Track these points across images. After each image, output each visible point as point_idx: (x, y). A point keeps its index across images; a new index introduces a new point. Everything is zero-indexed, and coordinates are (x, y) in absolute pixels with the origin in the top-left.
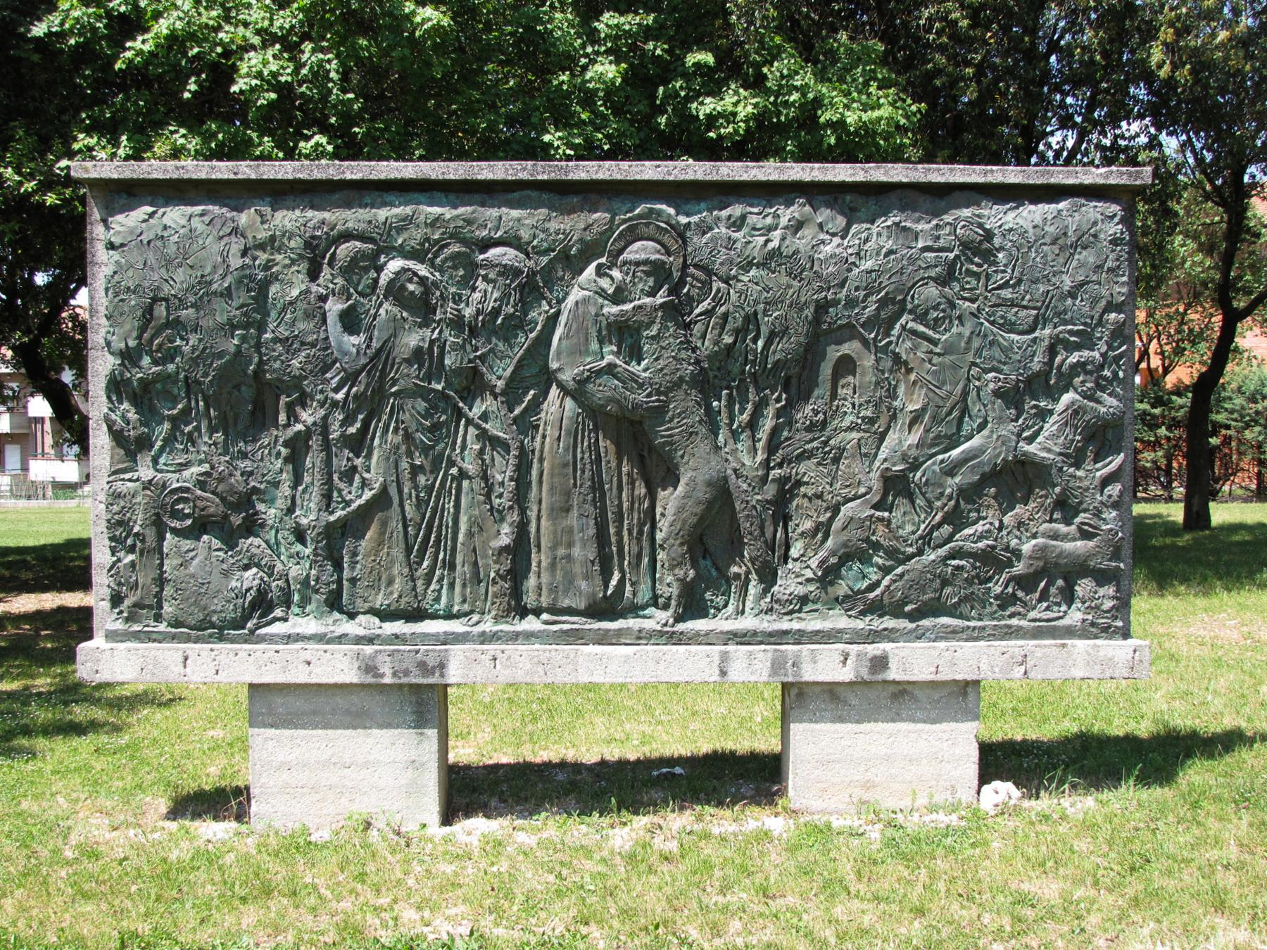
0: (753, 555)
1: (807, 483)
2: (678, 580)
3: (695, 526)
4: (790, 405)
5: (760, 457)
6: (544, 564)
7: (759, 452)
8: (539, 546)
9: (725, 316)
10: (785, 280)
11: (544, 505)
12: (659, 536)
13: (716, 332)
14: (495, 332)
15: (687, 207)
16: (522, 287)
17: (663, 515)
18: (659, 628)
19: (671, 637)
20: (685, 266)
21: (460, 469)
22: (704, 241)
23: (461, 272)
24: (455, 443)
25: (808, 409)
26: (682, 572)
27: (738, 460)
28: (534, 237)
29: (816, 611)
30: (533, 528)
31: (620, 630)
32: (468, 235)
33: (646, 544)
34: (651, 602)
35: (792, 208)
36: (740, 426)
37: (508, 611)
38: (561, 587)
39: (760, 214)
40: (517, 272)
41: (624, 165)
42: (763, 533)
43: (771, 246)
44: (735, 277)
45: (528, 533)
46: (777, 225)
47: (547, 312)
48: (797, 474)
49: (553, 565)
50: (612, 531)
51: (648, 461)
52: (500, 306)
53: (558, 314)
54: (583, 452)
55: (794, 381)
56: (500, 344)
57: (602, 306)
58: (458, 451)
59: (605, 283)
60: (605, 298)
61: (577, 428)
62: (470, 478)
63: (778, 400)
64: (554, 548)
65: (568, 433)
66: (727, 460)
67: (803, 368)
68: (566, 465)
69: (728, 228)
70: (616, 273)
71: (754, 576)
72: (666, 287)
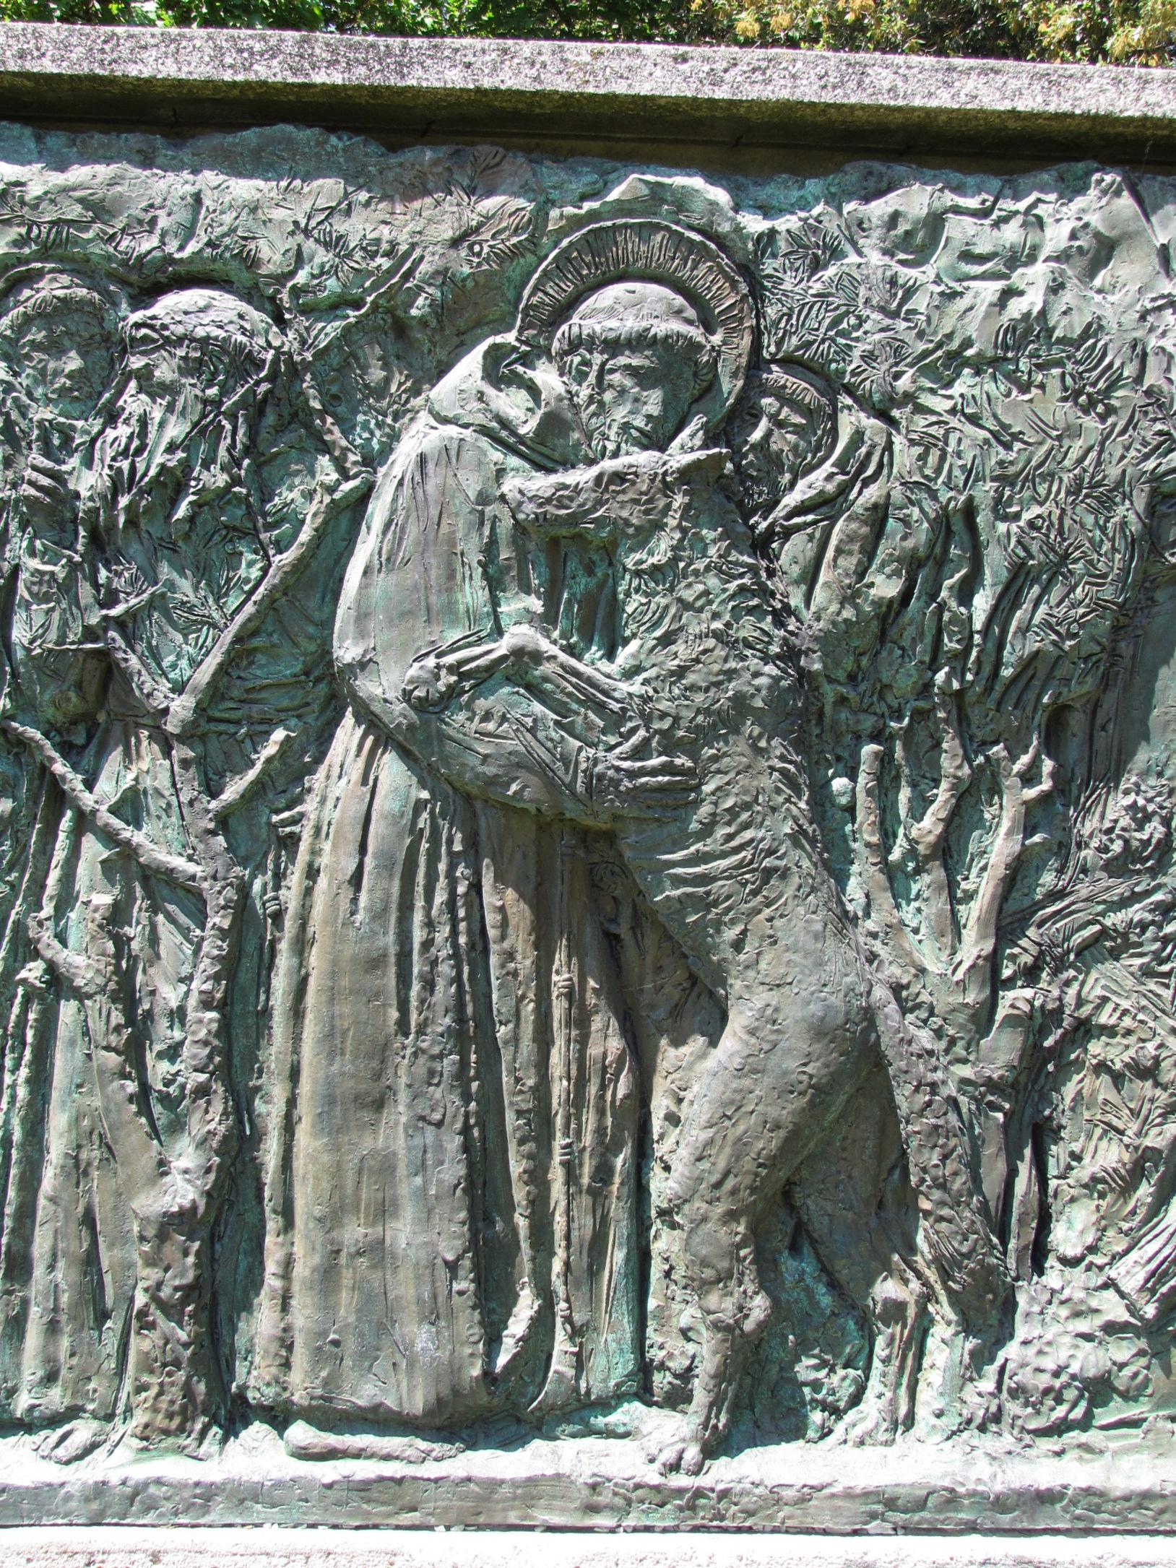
0: (947, 1250)
1: (1111, 1031)
2: (717, 1326)
3: (772, 1163)
4: (1064, 790)
5: (973, 947)
6: (301, 1271)
7: (969, 934)
8: (287, 1212)
9: (879, 515)
10: (1058, 411)
11: (305, 1087)
12: (662, 1187)
13: (849, 563)
14: (167, 547)
15: (770, 192)
16: (256, 409)
17: (673, 1119)
18: (652, 1476)
19: (692, 1507)
20: (756, 363)
21: (51, 968)
22: (817, 287)
23: (73, 362)
24: (38, 885)
25: (1117, 806)
26: (729, 1304)
27: (906, 958)
28: (300, 259)
29: (1134, 1423)
30: (270, 1154)
31: (531, 1481)
32: (97, 249)
33: (618, 1210)
34: (633, 1386)
35: (1080, 202)
36: (912, 853)
37: (186, 1415)
38: (351, 1344)
39: (984, 213)
40: (243, 362)
41: (580, 51)
42: (976, 1180)
43: (1016, 308)
44: (909, 397)
45: (258, 1168)
46: (1035, 248)
47: (331, 490)
48: (1080, 1002)
49: (328, 1275)
50: (517, 1167)
51: (630, 953)
52: (186, 466)
53: (363, 498)
54: (430, 924)
55: (1077, 721)
56: (185, 585)
57: (500, 473)
58: (48, 909)
59: (512, 404)
60: (511, 450)
61: (412, 852)
62: (79, 995)
63: (1029, 777)
64: (331, 1220)
65: (386, 864)
66: (872, 957)
67: (1106, 682)
68: (375, 963)
69: (885, 252)
70: (546, 376)
71: (943, 1310)
72: (696, 422)
